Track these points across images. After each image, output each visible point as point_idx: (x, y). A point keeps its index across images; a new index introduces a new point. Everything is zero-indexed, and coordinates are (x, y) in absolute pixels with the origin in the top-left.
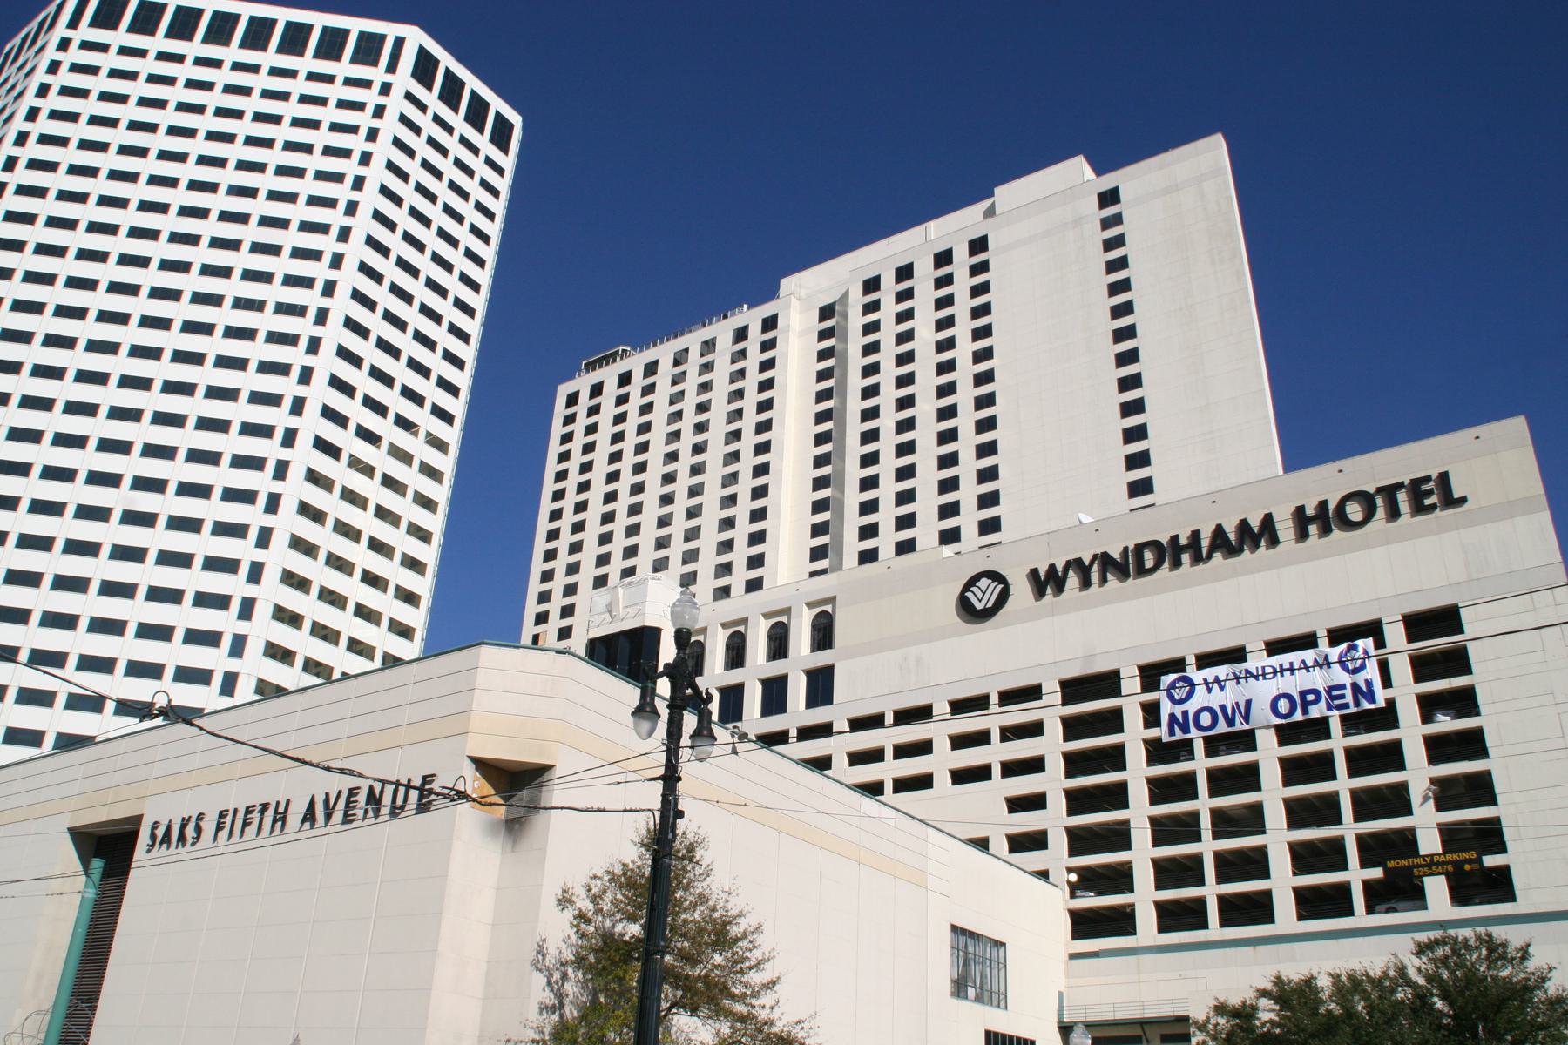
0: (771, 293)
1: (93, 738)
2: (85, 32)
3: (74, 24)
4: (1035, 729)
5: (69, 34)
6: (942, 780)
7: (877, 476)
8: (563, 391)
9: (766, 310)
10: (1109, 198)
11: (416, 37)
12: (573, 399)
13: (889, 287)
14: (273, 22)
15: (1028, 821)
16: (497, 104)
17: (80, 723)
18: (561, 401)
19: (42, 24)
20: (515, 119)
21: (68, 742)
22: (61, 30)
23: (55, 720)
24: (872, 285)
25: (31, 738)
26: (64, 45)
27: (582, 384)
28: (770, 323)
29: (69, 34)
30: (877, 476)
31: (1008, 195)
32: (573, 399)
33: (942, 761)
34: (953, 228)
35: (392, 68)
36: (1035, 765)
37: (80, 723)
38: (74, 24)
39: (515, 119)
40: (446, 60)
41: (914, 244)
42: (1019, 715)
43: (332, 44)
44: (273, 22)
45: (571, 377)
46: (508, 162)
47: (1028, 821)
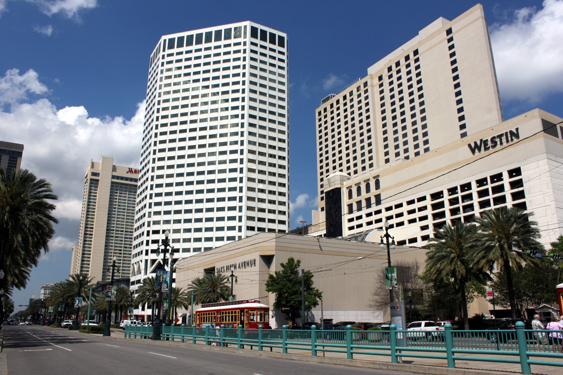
0: (365, 74)
1: (212, 248)
2: (168, 52)
3: (164, 50)
4: (425, 208)
5: (164, 53)
6: (406, 223)
7: (459, 83)
8: (317, 111)
9: (364, 80)
10: (449, 32)
11: (248, 24)
12: (320, 113)
13: (394, 69)
14: (211, 32)
15: (425, 233)
16: (278, 33)
17: (209, 244)
18: (317, 114)
19: (157, 49)
20: (284, 35)
21: (207, 249)
22: (162, 53)
23: (203, 245)
24: (390, 69)
25: (199, 249)
26: (163, 57)
27: (321, 109)
28: (366, 84)
29: (164, 53)
30: (459, 83)
31: (424, 33)
32: (320, 113)
33: (406, 218)
34: (407, 48)
35: (245, 37)
36: (425, 218)
37: (209, 244)
38: (164, 50)
39: (284, 35)
40: (260, 27)
41: (398, 54)
42: (422, 204)
43: (228, 35)
44: (211, 32)
45: (319, 106)
46: (284, 50)
47: (425, 233)
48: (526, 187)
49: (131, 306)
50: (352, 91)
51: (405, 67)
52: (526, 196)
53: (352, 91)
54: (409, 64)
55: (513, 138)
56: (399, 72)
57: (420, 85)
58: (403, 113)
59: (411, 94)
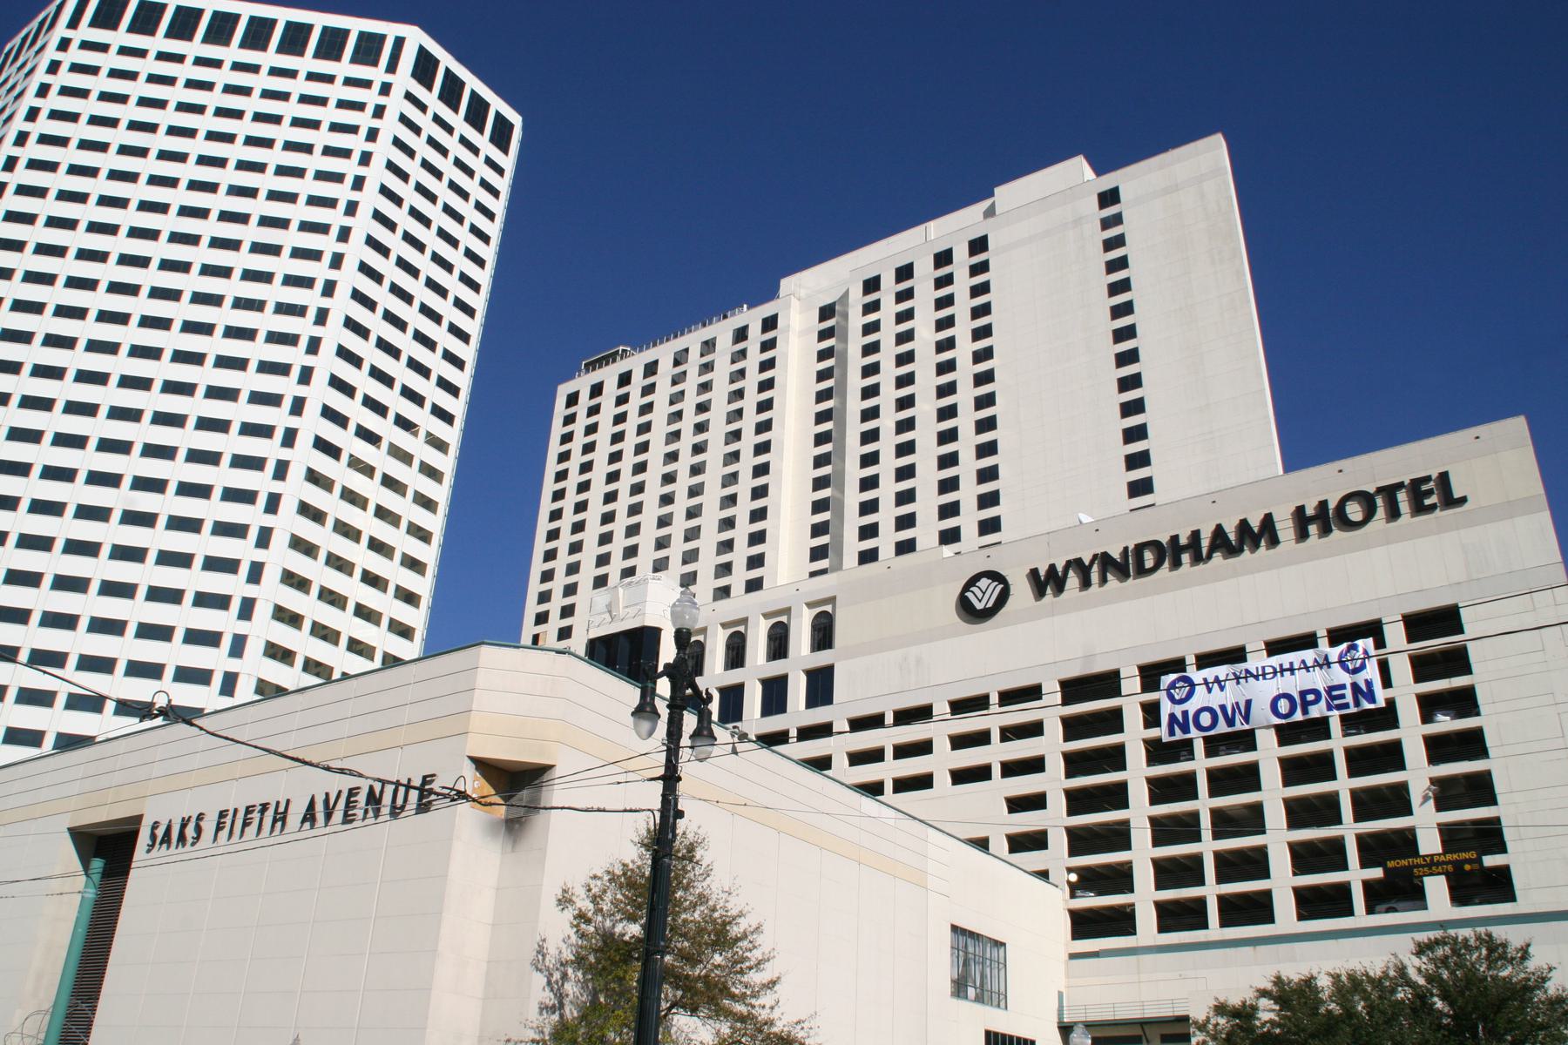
0: (771, 293)
2: (85, 32)
3: (74, 24)
4: (1035, 729)
5: (69, 34)
6: (942, 780)
8: (563, 391)
9: (766, 310)
10: (1109, 198)
11: (416, 37)
12: (573, 399)
13: (889, 287)
14: (273, 22)
15: (1028, 821)
16: (497, 104)
18: (561, 401)
19: (42, 24)
20: (515, 119)
22: (61, 30)
24: (872, 285)
26: (64, 45)
27: (582, 384)
28: (770, 323)
29: (69, 34)
31: (1008, 195)
32: (573, 399)
33: (942, 761)
34: (953, 228)
36: (1035, 765)
38: (74, 24)
39: (515, 119)
40: (446, 60)
41: (914, 244)
42: (1019, 715)
43: (332, 44)
44: (273, 22)
45: (571, 377)
46: (508, 162)
47: (1028, 821)
48: (1483, 677)
49: (1250, 1030)
50: (656, 362)
51: (614, 401)
52: (1482, 709)
53: (656, 362)
54: (574, 415)
55: (1110, 577)
56: (648, 390)
57: (641, 458)
58: (578, 527)
59: (613, 477)
